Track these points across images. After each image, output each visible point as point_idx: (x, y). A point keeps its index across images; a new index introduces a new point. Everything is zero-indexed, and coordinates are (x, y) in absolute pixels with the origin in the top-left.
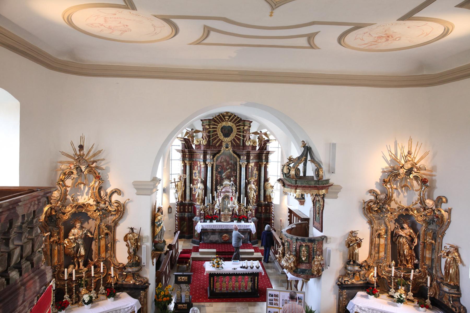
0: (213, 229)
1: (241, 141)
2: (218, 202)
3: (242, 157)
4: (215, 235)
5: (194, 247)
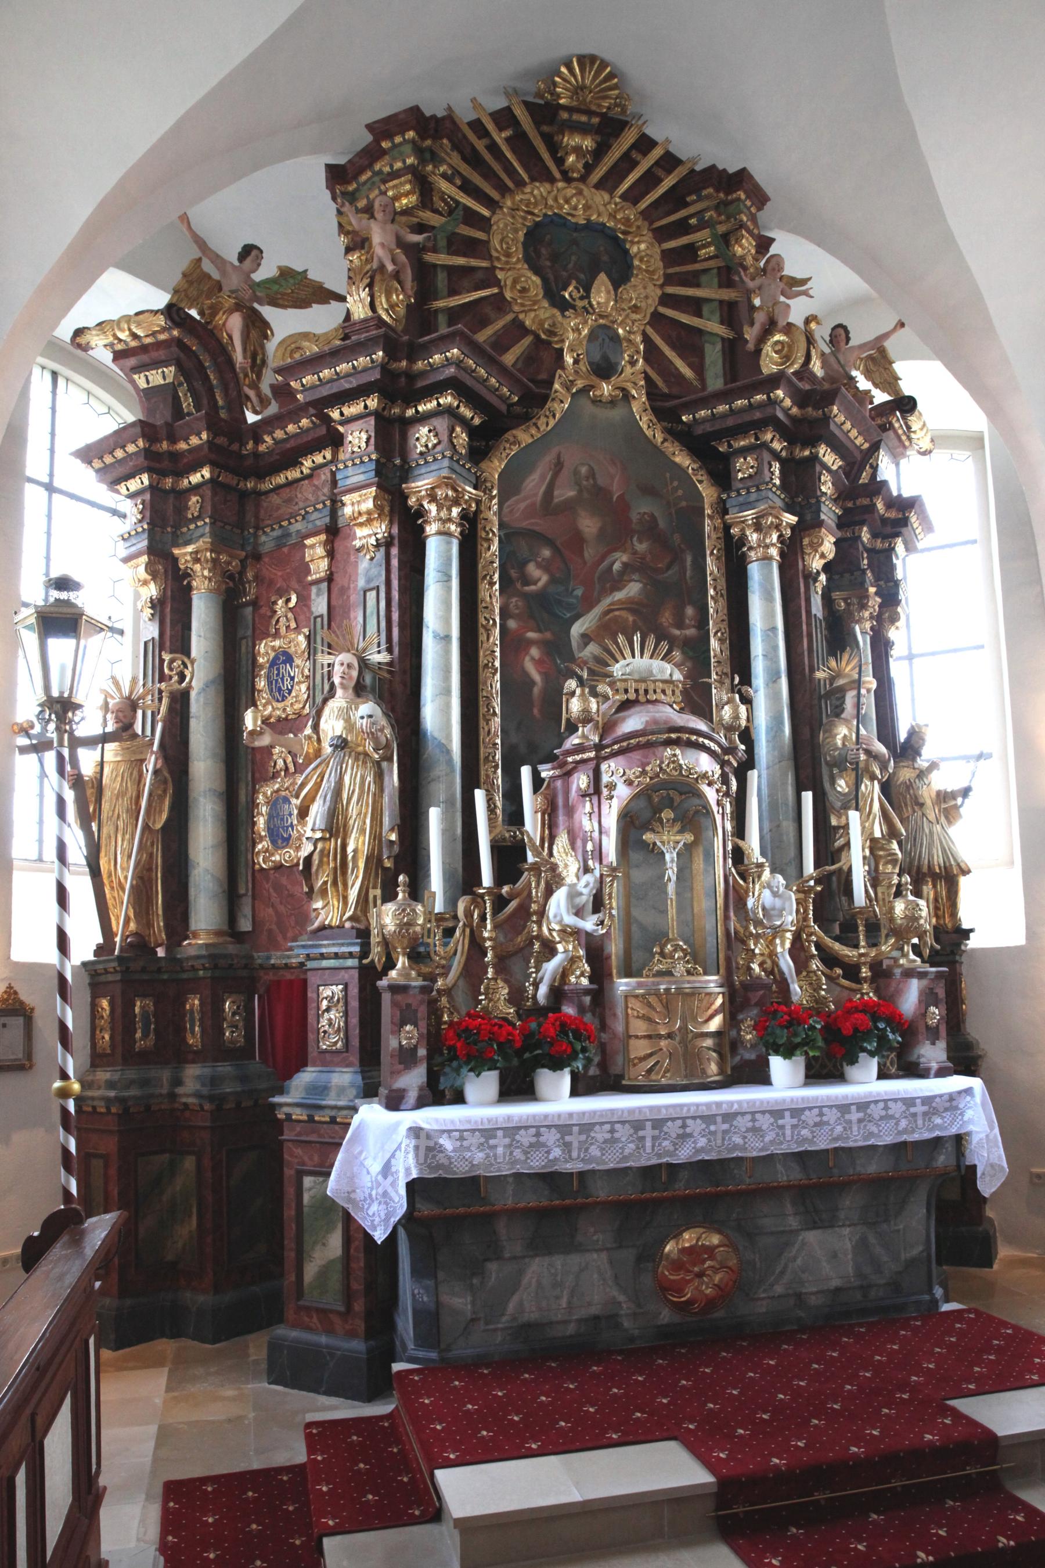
0: (551, 1179)
1: (713, 354)
2: (568, 863)
3: (744, 467)
4: (572, 1247)
5: (319, 1435)
